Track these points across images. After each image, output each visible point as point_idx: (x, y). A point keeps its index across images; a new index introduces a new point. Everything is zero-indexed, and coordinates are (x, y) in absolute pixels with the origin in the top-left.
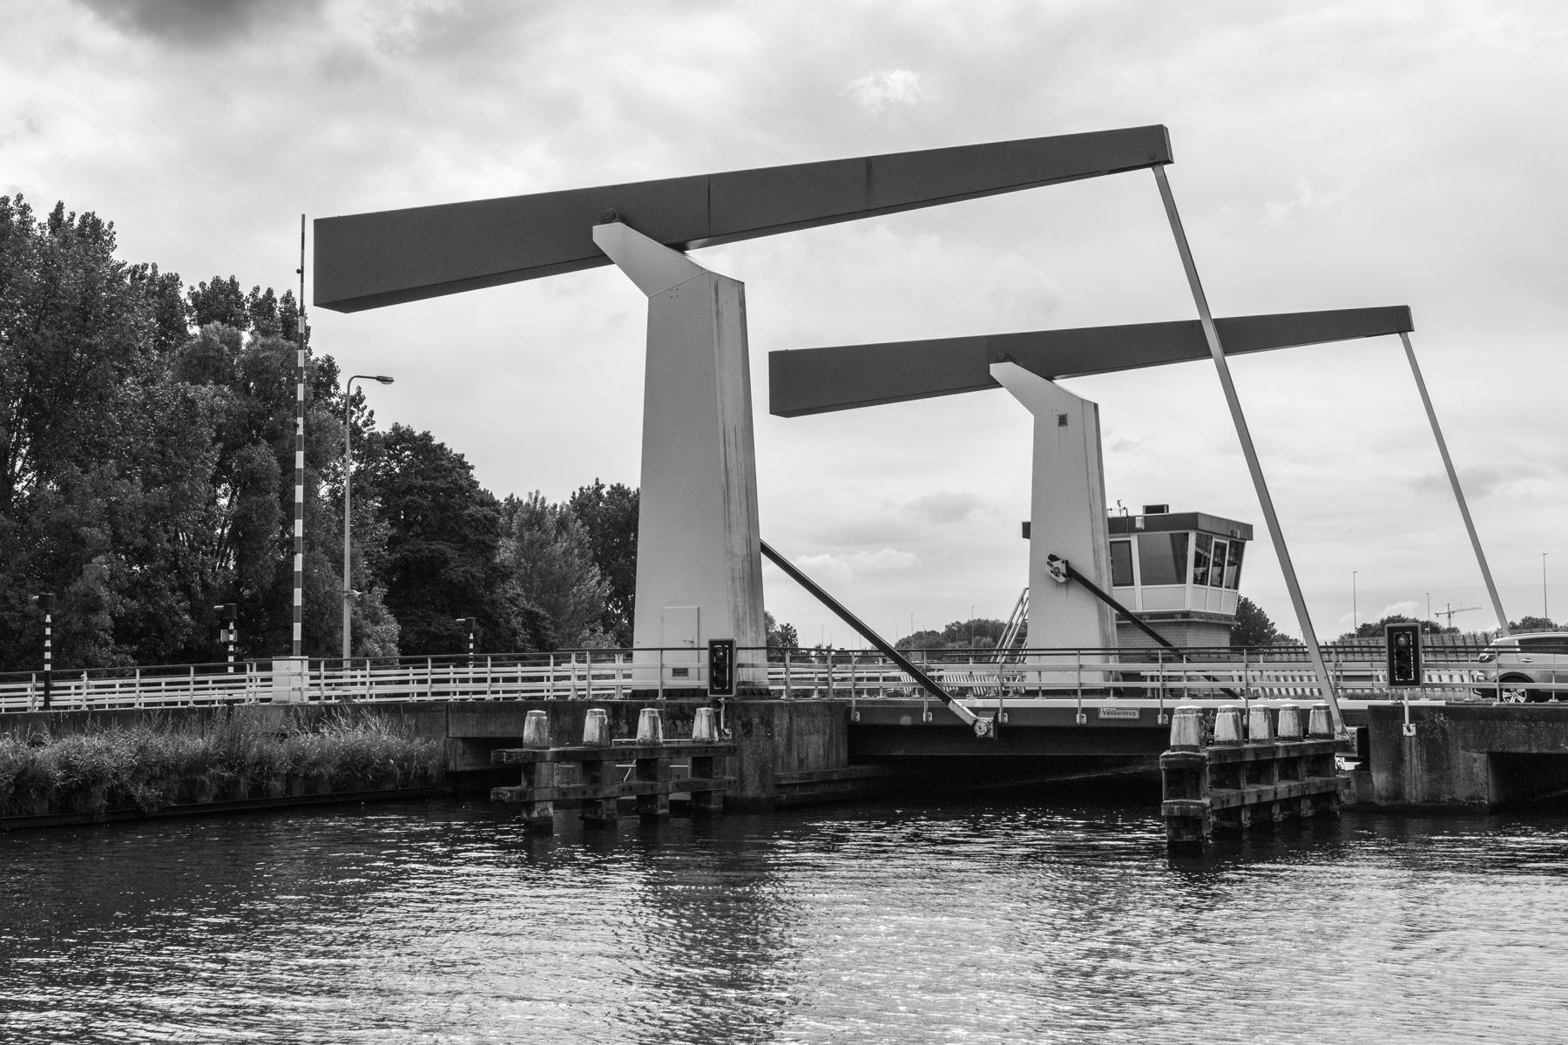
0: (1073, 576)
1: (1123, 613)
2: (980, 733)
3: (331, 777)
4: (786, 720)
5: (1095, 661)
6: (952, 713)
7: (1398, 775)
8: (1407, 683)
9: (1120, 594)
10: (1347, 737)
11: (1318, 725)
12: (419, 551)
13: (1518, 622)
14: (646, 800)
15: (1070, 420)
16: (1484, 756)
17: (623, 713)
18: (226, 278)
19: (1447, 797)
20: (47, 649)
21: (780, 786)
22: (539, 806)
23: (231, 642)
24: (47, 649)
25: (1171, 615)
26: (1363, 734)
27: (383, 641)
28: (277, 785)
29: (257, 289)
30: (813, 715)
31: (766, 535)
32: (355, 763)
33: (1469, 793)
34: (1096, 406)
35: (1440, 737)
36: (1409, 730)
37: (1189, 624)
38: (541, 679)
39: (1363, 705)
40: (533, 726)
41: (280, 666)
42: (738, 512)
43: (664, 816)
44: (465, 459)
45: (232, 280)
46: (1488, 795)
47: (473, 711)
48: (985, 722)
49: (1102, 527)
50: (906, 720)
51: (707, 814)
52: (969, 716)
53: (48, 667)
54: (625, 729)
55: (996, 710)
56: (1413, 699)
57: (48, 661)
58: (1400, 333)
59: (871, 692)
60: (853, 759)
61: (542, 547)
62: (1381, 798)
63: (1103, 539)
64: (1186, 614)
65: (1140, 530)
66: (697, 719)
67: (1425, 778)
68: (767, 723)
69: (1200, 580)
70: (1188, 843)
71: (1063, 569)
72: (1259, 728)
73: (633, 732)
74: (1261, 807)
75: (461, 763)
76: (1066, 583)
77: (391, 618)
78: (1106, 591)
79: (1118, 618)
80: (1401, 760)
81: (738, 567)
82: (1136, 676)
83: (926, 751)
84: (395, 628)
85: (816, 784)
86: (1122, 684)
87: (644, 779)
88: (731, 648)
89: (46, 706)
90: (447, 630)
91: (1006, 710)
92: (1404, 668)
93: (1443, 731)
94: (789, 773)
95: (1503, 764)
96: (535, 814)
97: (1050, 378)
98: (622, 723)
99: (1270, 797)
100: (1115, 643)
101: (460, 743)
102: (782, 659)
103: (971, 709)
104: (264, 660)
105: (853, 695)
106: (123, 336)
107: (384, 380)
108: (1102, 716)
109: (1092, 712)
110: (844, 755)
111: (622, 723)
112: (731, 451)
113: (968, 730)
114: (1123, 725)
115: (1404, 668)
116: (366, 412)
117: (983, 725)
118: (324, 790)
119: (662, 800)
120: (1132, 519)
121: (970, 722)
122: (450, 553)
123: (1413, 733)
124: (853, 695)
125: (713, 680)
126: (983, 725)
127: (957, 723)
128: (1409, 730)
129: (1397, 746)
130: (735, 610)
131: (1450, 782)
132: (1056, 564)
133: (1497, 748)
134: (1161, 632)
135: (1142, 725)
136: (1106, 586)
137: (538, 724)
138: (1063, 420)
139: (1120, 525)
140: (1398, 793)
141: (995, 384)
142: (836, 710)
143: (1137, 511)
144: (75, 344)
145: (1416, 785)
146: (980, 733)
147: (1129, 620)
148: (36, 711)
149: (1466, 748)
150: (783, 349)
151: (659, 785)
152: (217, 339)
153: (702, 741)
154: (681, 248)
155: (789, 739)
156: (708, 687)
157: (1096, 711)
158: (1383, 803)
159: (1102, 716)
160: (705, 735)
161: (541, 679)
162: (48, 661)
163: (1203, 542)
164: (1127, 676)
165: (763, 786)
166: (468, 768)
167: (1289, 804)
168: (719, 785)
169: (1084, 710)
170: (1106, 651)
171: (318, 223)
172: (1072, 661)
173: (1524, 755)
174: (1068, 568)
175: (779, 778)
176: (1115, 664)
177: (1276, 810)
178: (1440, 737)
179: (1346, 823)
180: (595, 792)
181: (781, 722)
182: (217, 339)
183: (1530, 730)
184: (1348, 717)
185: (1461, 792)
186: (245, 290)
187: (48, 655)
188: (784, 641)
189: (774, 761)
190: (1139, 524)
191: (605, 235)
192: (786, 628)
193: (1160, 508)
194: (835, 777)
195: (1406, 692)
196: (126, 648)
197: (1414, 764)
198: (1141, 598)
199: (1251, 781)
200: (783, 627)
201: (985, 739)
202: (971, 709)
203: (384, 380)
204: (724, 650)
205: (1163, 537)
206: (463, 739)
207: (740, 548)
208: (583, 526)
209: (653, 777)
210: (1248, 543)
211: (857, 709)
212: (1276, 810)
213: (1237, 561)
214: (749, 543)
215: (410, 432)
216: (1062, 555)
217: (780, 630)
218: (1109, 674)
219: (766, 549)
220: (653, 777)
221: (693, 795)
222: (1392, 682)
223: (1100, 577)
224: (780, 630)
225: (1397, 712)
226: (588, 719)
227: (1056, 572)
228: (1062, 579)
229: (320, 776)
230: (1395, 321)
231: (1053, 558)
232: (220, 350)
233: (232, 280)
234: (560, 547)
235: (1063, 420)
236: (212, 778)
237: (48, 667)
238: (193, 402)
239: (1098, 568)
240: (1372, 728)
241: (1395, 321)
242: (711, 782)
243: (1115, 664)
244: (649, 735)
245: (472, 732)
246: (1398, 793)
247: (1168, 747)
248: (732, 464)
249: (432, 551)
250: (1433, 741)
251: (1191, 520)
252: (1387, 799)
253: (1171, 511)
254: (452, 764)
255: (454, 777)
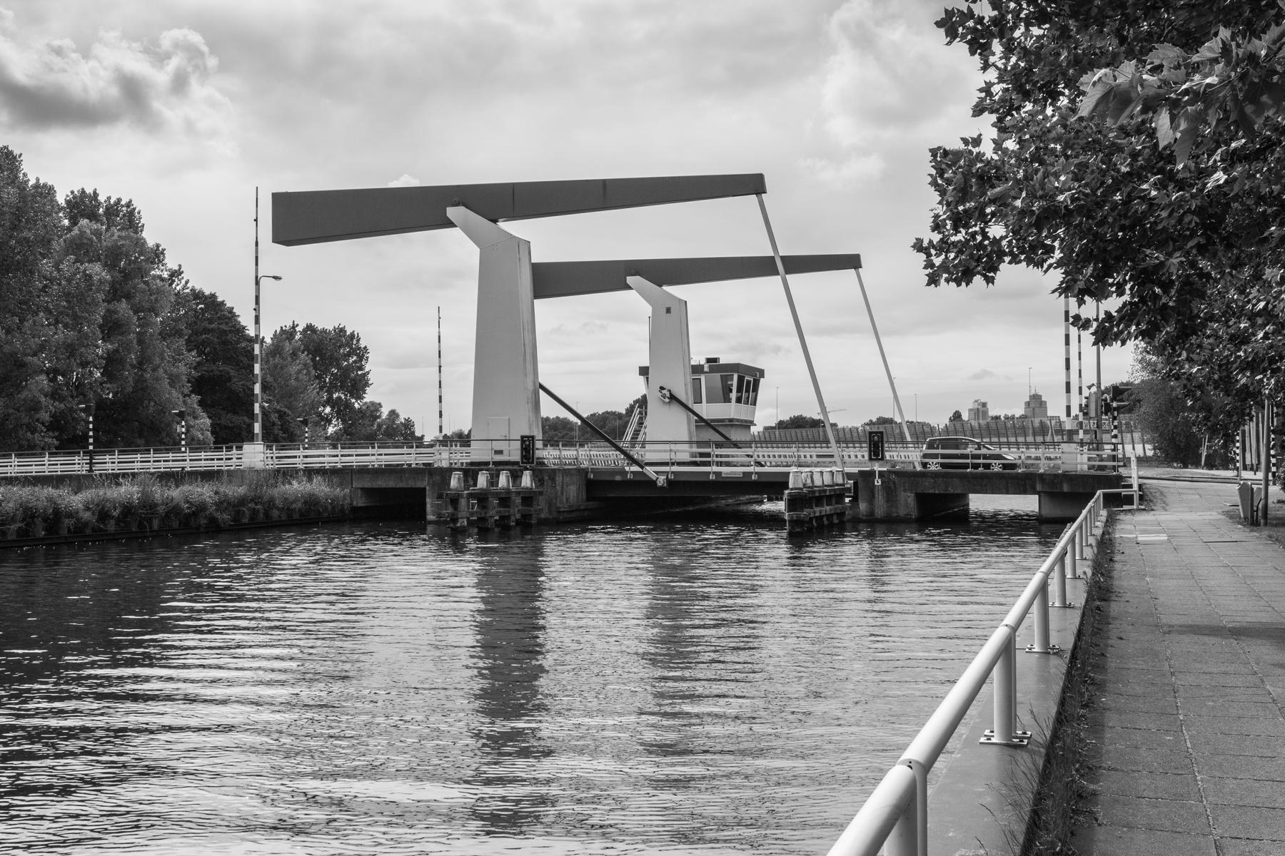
0: (673, 398)
1: (701, 419)
2: (659, 484)
3: (300, 510)
4: (561, 478)
5: (686, 447)
6: (645, 474)
7: (872, 504)
8: (877, 460)
9: (696, 408)
10: (849, 486)
11: (839, 480)
12: (212, 371)
13: (874, 420)
14: (482, 519)
15: (672, 310)
16: (913, 495)
17: (470, 472)
18: (89, 191)
19: (895, 514)
20: (91, 437)
21: (559, 512)
22: (460, 521)
23: (183, 433)
24: (91, 437)
25: (723, 420)
26: (856, 484)
27: (202, 430)
28: (275, 513)
29: (109, 198)
30: (572, 475)
31: (542, 380)
32: (311, 502)
33: (905, 513)
34: (686, 302)
35: (892, 486)
36: (878, 482)
37: (732, 425)
38: (295, 457)
39: (855, 470)
40: (456, 480)
41: (247, 447)
42: (529, 366)
43: (513, 526)
44: (234, 311)
45: (95, 192)
46: (914, 514)
47: (368, 473)
48: (662, 478)
49: (689, 370)
50: (618, 478)
51: (530, 526)
52: (654, 476)
53: (91, 448)
54: (471, 483)
55: (668, 472)
56: (877, 467)
57: (91, 444)
58: (756, 194)
59: (976, 466)
60: (588, 499)
61: (282, 368)
62: (863, 515)
63: (690, 377)
64: (731, 420)
65: (707, 372)
66: (524, 477)
67: (885, 506)
68: (553, 479)
69: (739, 400)
70: (798, 532)
71: (668, 395)
72: (818, 482)
73: (475, 484)
74: (820, 518)
75: (360, 502)
76: (669, 402)
77: (205, 415)
78: (690, 406)
79: (696, 421)
80: (873, 497)
81: (530, 396)
82: (708, 455)
83: (631, 494)
84: (208, 421)
85: (573, 511)
86: (698, 459)
87: (504, 507)
88: (533, 440)
89: (91, 470)
90: (232, 423)
91: (672, 472)
92: (876, 451)
93: (894, 483)
94: (564, 507)
95: (922, 499)
96: (459, 525)
97: (660, 286)
98: (470, 480)
99: (823, 513)
100: (694, 439)
101: (359, 491)
102: (558, 446)
103: (655, 472)
104: (239, 444)
105: (1134, 464)
106: (47, 233)
107: (276, 278)
108: (723, 475)
109: (718, 474)
110: (585, 497)
111: (470, 480)
112: (526, 334)
113: (654, 483)
114: (727, 480)
115: (876, 451)
116: (183, 282)
117: (661, 480)
118: (296, 516)
119: (513, 518)
120: (702, 366)
121: (655, 479)
122: (232, 373)
123: (880, 483)
124: (1134, 464)
125: (523, 457)
126: (661, 480)
127: (647, 479)
128: (878, 482)
129: (871, 489)
130: (529, 420)
131: (897, 507)
132: (664, 392)
133: (919, 491)
134: (720, 429)
135: (743, 480)
136: (690, 404)
137: (459, 479)
138: (668, 310)
139: (697, 369)
140: (871, 513)
141: (450, 224)
142: (583, 472)
143: (703, 362)
144: (11, 237)
145: (881, 508)
146: (659, 484)
147: (703, 423)
148: (84, 472)
149: (905, 491)
150: (285, 191)
151: (512, 511)
152: (88, 231)
153: (527, 488)
154: (495, 221)
155: (562, 488)
156: (519, 460)
157: (721, 473)
158: (864, 518)
159: (723, 475)
160: (529, 485)
161: (295, 457)
162: (91, 444)
163: (741, 379)
164: (702, 455)
165: (550, 512)
166: (363, 505)
167: (829, 516)
168: (536, 511)
169: (714, 473)
170: (690, 442)
171: (279, 199)
172: (667, 447)
173: (931, 494)
174: (671, 394)
175: (559, 508)
176: (695, 449)
177: (825, 519)
178: (892, 486)
179: (848, 526)
180: (485, 513)
181: (559, 479)
182: (88, 231)
183: (935, 482)
184: (849, 476)
185: (902, 512)
186: (102, 198)
187: (91, 440)
188: (406, 429)
189: (556, 498)
190: (706, 369)
191: (452, 212)
192: (408, 420)
193: (715, 360)
194: (582, 508)
195: (877, 464)
196: (51, 434)
197: (880, 499)
198: (709, 410)
199: (817, 506)
200: (405, 419)
201: (662, 487)
202: (655, 472)
203: (276, 278)
204: (529, 441)
205: (717, 376)
206: (362, 489)
207: (530, 387)
208: (307, 355)
209: (508, 506)
210: (762, 379)
211: (591, 472)
212: (825, 519)
213: (756, 390)
214: (534, 383)
215: (201, 292)
216: (668, 388)
217: (403, 421)
218: (693, 455)
219: (542, 387)
220: (508, 506)
221: (522, 515)
222: (870, 459)
223: (688, 399)
224: (403, 421)
225: (872, 473)
226: (479, 476)
227: (664, 396)
228: (667, 400)
229: (295, 508)
230: (852, 262)
231: (662, 388)
232: (91, 240)
233: (95, 192)
234: (294, 369)
235: (668, 310)
236: (249, 509)
237: (91, 448)
238: (90, 276)
239: (687, 394)
240: (859, 482)
241: (852, 262)
242: (532, 509)
243: (695, 449)
244: (505, 485)
245: (367, 485)
246: (871, 513)
247: (787, 488)
248: (527, 342)
249: (221, 371)
250: (889, 487)
251: (736, 367)
252: (867, 516)
253: (721, 362)
254: (355, 503)
255: (355, 510)
